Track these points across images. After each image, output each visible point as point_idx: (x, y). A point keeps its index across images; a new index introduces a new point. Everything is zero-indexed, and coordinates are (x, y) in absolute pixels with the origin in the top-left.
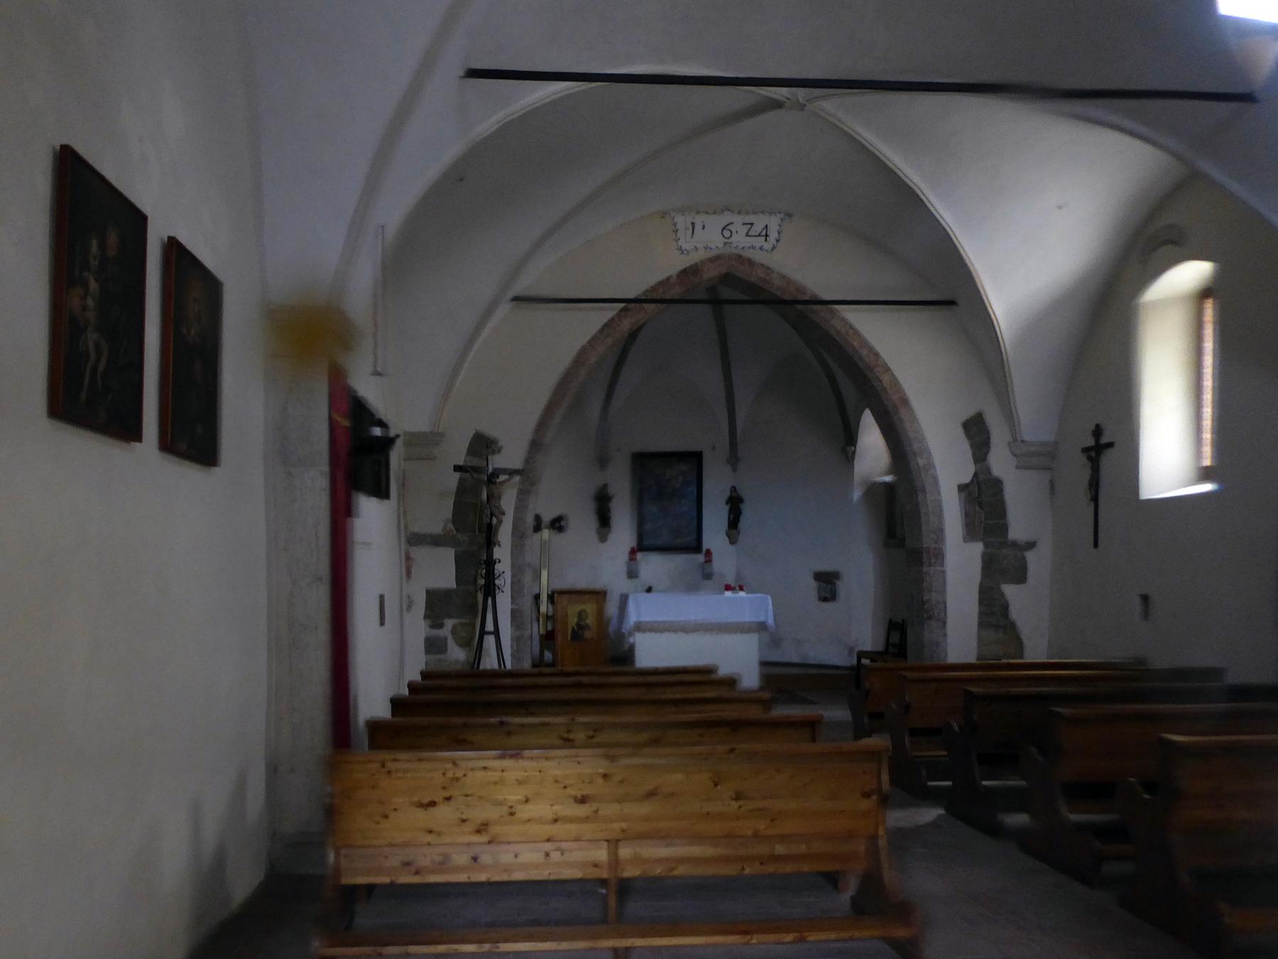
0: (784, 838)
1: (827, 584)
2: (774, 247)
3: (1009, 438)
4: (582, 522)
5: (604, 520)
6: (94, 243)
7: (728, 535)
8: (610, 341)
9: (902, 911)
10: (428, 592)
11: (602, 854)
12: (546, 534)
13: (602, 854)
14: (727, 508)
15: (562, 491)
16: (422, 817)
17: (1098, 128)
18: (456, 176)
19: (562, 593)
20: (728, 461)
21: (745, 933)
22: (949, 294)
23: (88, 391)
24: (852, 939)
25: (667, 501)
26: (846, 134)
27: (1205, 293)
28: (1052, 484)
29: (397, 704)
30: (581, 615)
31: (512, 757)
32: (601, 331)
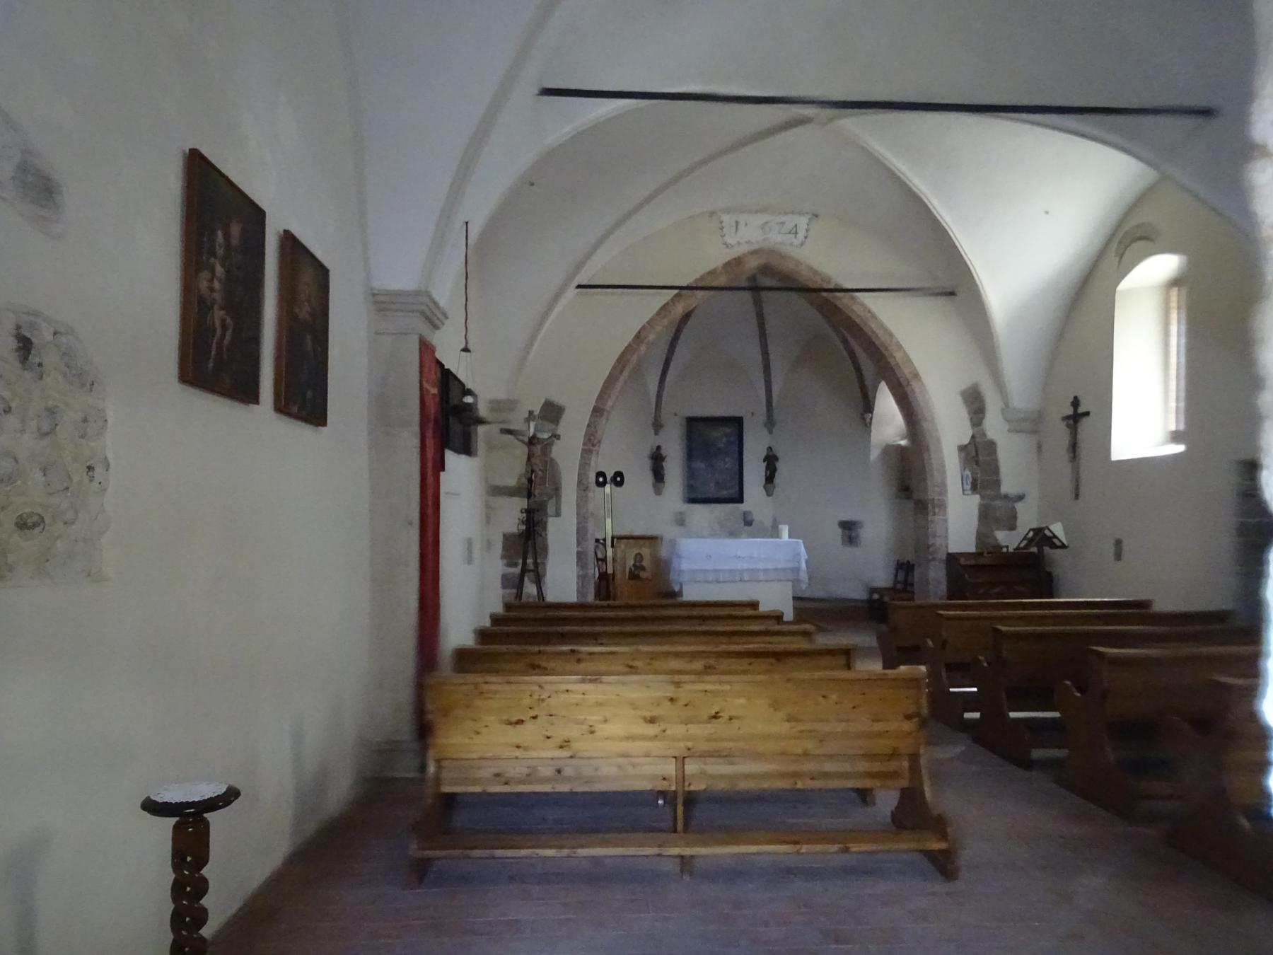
0: (831, 757)
1: (849, 530)
2: (802, 244)
3: (1001, 405)
4: (638, 476)
5: (658, 475)
6: (220, 234)
7: (765, 487)
8: (665, 322)
9: (939, 825)
10: (504, 535)
11: (670, 769)
12: (608, 488)
13: (670, 769)
14: (764, 465)
15: (623, 449)
16: (514, 735)
17: (1056, 133)
18: (529, 182)
19: (620, 538)
20: (766, 425)
21: (796, 843)
22: (953, 286)
23: (214, 359)
24: (889, 851)
25: (713, 459)
26: (863, 149)
27: (1176, 282)
28: (1039, 447)
29: (482, 635)
30: (639, 557)
31: (591, 681)
32: (658, 313)
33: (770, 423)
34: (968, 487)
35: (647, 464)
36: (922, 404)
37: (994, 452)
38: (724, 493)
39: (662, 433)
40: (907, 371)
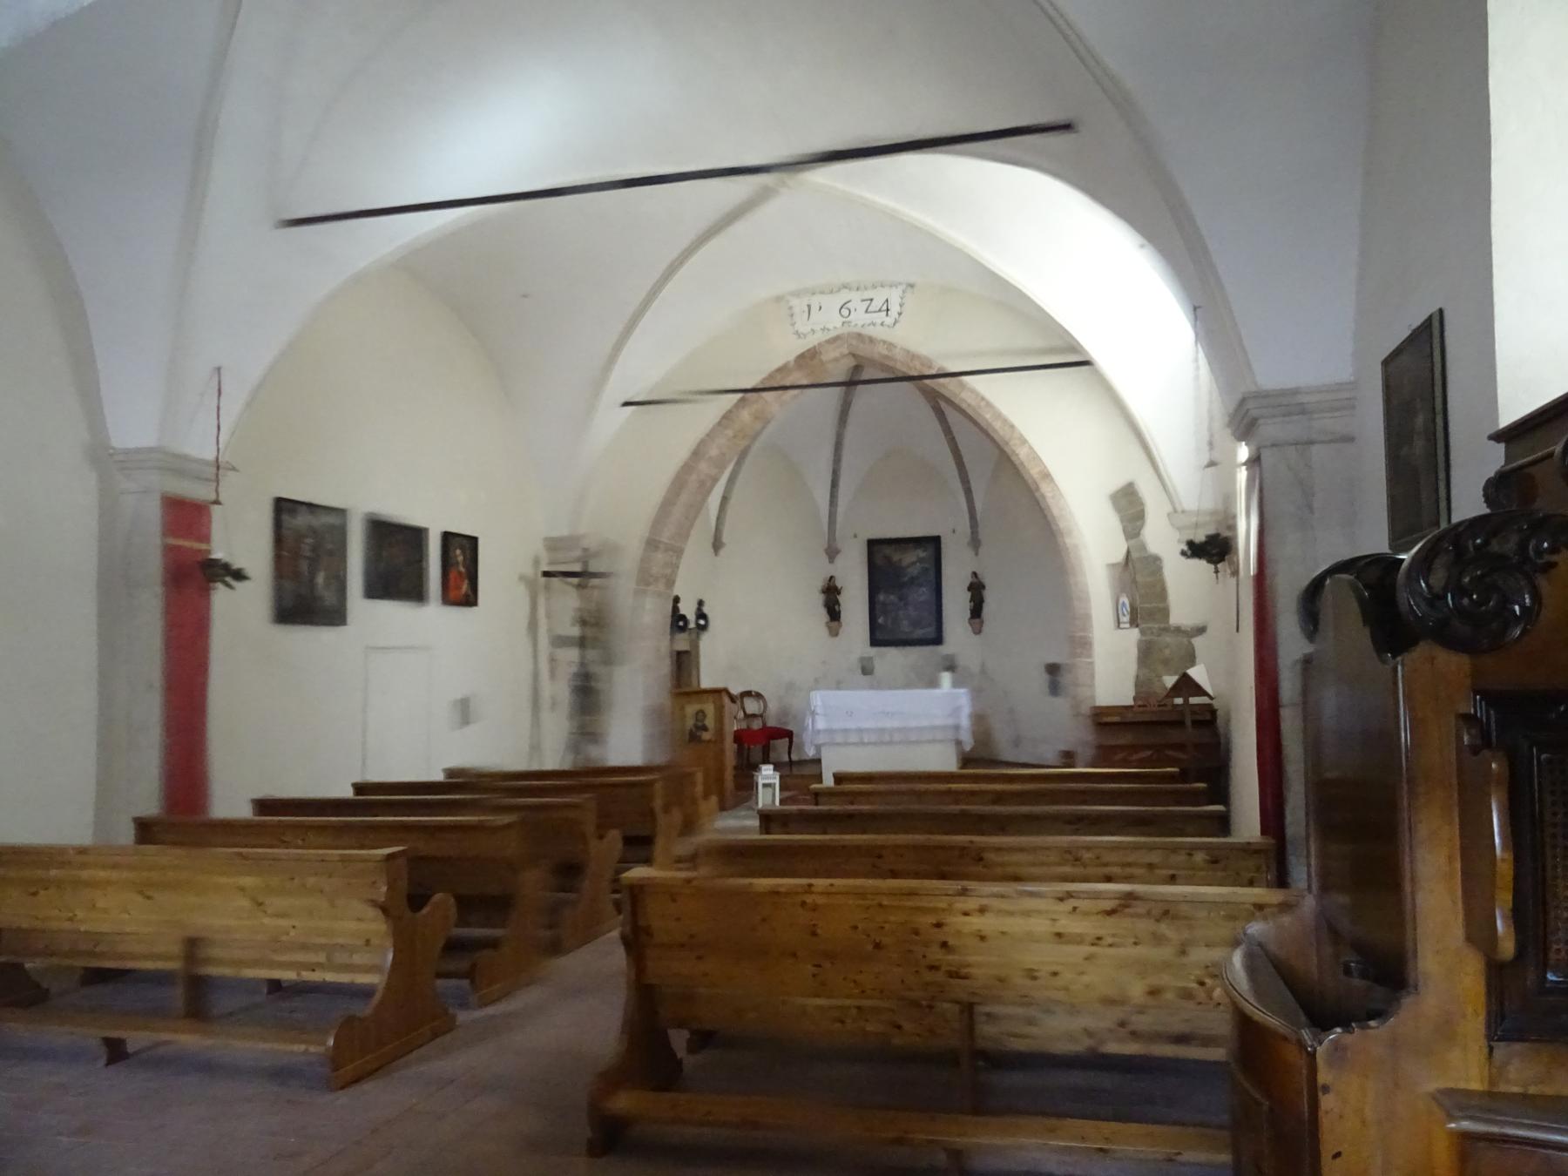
14: (969, 595)
33: (975, 543)
34: (1126, 619)
35: (819, 599)
36: (1055, 512)
37: (1160, 569)
38: (919, 633)
39: (839, 560)
40: (1035, 472)
